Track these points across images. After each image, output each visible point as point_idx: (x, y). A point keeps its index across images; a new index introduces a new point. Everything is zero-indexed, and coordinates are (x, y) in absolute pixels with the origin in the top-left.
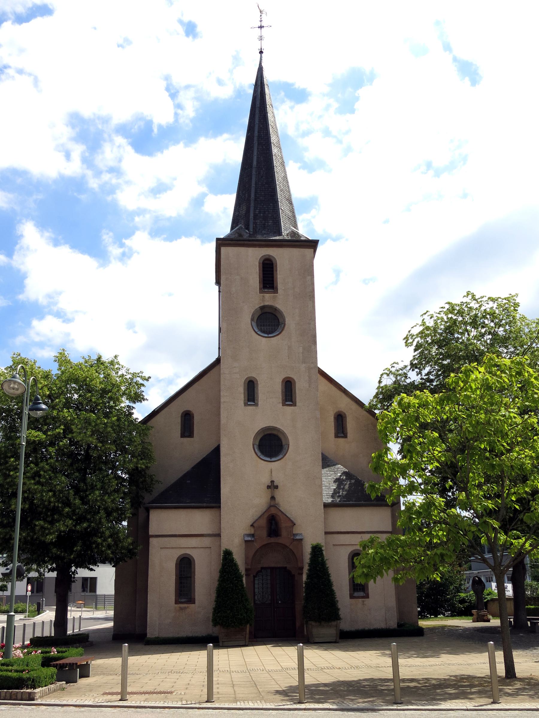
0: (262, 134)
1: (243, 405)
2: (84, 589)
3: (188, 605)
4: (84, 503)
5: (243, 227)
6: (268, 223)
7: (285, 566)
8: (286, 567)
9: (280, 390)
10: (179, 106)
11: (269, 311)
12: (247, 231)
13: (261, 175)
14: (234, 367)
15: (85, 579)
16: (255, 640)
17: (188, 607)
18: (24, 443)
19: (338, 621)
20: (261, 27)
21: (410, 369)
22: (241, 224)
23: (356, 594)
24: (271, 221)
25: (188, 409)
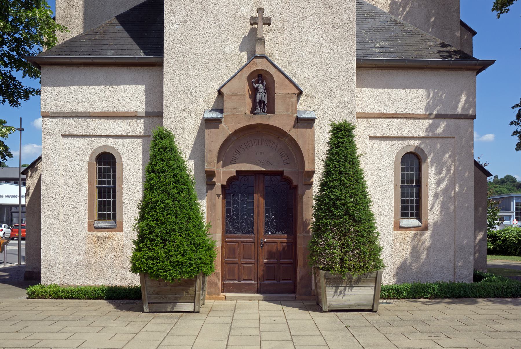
3: (111, 233)
7: (280, 169)
8: (282, 173)
10: (418, 321)
16: (223, 295)
17: (111, 237)
23: (405, 222)
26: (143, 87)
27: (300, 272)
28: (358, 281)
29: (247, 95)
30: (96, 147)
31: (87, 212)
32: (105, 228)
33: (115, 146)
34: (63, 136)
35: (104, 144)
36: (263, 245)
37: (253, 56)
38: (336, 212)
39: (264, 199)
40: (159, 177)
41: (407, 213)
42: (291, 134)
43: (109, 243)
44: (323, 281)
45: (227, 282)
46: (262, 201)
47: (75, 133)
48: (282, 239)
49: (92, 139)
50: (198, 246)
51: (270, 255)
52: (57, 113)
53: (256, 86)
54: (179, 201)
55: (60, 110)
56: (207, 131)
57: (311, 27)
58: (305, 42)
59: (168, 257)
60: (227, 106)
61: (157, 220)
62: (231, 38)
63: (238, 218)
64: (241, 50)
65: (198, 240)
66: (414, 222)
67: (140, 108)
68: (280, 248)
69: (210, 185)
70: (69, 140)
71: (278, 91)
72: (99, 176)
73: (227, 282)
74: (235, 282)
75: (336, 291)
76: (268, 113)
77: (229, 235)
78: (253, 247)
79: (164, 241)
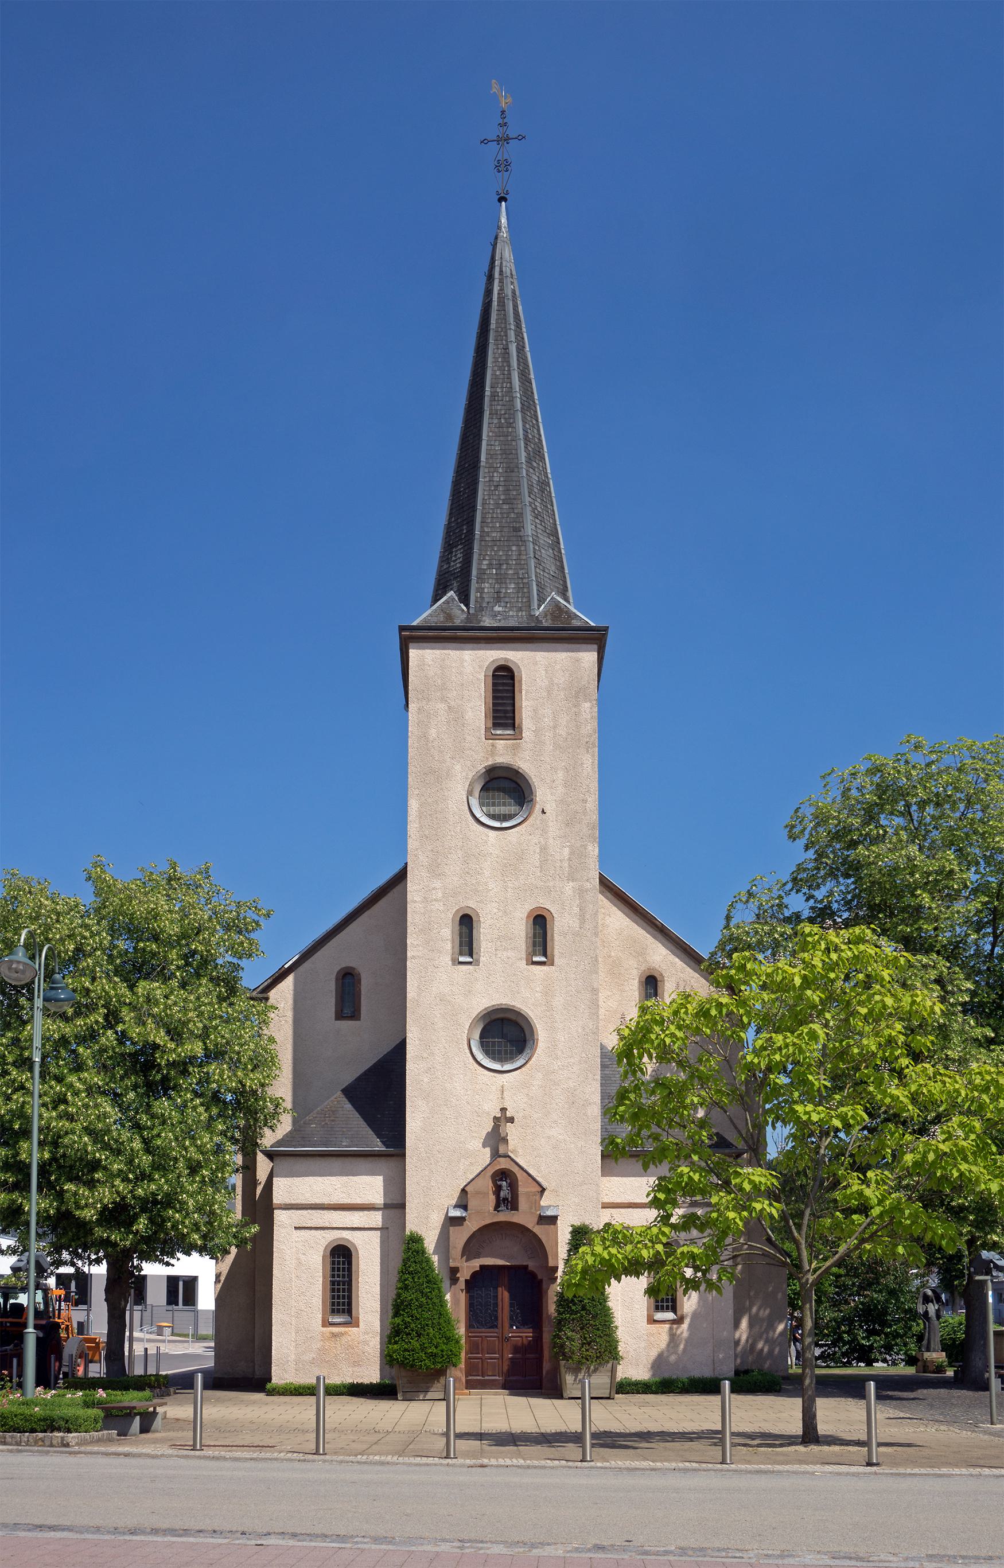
0: (499, 390)
1: (450, 962)
2: (172, 1299)
3: (347, 1329)
4: (148, 1150)
5: (456, 598)
6: (507, 588)
8: (526, 1267)
9: (523, 934)
11: (504, 775)
12: (465, 608)
13: (495, 484)
14: (433, 889)
15: (172, 1281)
16: (467, 1391)
17: (346, 1333)
18: (37, 1060)
19: (615, 1362)
20: (504, 140)
21: (791, 890)
22: (451, 589)
23: (659, 1316)
24: (513, 586)
25: (351, 965)
26: (381, 1178)
27: (546, 1366)
28: (595, 1370)
29: (491, 1192)
30: (331, 1239)
31: (321, 1307)
32: (340, 1324)
33: (351, 1239)
34: (296, 1228)
35: (339, 1236)
36: (508, 1339)
37: (496, 1155)
38: (574, 1308)
39: (509, 1292)
40: (413, 1278)
41: (662, 1306)
42: (534, 1230)
43: (344, 1339)
44: (563, 1370)
45: (470, 1378)
46: (506, 1295)
47: (309, 1225)
48: (528, 1334)
49: (326, 1231)
50: (448, 1338)
51: (516, 1349)
52: (290, 1204)
53: (499, 1183)
54: (431, 1299)
55: (293, 1202)
56: (451, 1228)
57: (555, 1122)
58: (549, 1137)
59: (423, 1348)
60: (472, 1204)
61: (412, 1316)
62: (474, 1134)
63: (481, 1312)
64: (484, 1146)
65: (448, 1334)
66: (670, 1315)
67: (379, 1199)
68: (525, 1342)
69: (454, 1280)
70: (303, 1232)
71: (521, 1190)
72: (333, 1269)
73: (470, 1378)
74: (478, 1378)
75: (575, 1380)
76: (512, 1210)
77: (472, 1330)
78: (497, 1343)
79: (419, 1335)
